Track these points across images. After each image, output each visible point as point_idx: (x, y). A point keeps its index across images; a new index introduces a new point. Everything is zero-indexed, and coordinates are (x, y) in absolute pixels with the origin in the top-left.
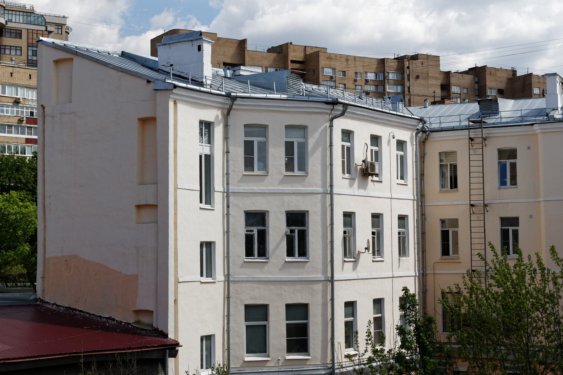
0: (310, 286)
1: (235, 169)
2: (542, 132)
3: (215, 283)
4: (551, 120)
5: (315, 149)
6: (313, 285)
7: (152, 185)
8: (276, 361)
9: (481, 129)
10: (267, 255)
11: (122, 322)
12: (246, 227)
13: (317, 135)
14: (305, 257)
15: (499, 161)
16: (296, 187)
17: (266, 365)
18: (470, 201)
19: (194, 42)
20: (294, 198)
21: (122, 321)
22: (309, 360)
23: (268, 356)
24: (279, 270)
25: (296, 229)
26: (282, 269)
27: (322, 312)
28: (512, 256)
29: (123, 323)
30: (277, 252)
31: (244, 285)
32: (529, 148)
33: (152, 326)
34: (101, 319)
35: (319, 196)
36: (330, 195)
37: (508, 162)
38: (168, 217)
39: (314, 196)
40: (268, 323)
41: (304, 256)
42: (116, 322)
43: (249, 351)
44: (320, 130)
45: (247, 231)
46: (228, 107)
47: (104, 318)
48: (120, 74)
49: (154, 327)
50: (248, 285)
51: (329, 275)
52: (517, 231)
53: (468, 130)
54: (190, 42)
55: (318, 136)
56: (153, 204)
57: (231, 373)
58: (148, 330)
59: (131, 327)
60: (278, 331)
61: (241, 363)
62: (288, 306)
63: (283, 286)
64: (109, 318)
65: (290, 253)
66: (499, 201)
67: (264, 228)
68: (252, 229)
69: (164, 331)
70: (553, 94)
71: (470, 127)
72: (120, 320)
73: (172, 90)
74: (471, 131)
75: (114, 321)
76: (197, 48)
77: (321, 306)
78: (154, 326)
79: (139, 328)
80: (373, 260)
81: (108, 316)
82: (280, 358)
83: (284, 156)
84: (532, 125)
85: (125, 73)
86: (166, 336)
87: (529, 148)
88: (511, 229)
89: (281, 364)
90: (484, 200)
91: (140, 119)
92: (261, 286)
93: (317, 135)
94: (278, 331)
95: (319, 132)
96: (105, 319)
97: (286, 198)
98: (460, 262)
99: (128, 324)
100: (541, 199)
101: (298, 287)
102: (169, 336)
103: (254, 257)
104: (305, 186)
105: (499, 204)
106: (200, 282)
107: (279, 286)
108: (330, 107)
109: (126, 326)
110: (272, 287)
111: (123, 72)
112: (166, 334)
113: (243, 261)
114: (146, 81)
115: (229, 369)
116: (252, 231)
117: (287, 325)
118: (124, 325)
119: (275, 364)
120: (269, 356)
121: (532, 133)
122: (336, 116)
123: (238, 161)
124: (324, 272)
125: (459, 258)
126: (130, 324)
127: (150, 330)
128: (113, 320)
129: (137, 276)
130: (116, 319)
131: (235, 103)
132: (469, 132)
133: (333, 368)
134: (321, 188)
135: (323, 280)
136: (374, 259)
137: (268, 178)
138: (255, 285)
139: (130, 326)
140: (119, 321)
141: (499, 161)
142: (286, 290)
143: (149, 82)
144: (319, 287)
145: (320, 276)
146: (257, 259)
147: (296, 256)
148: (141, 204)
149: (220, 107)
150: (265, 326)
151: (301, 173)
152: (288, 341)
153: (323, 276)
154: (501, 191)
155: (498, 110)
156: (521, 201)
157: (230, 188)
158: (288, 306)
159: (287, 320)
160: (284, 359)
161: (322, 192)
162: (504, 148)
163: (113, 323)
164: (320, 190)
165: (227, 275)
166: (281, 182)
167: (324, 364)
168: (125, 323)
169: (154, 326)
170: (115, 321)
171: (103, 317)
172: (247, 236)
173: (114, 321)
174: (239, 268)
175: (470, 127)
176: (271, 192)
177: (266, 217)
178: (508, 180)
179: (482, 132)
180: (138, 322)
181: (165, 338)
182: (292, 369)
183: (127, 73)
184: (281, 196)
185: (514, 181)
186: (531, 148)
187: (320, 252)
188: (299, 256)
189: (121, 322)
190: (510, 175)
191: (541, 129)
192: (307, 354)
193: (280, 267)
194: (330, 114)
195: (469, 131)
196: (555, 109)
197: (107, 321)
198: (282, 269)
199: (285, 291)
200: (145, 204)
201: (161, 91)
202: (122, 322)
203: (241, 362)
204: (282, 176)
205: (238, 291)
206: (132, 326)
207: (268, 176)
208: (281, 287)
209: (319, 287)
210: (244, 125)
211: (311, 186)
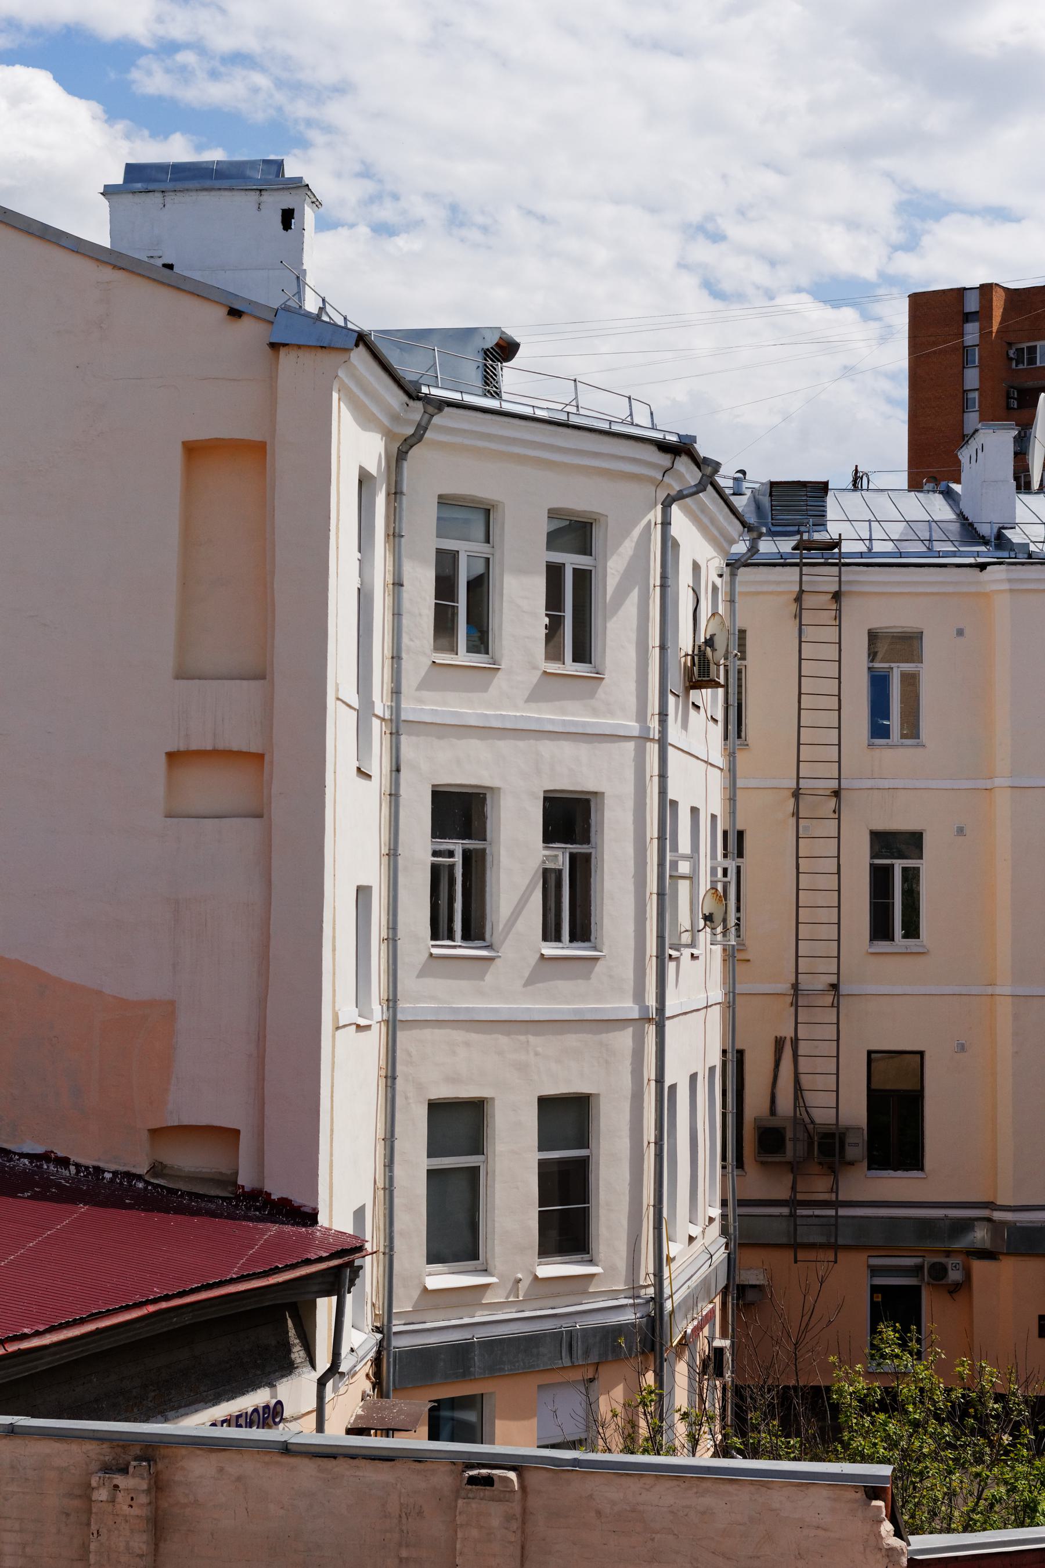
0: (604, 1037)
1: (412, 643)
2: (1011, 591)
3: (370, 1030)
4: (1020, 555)
5: (622, 593)
6: (611, 1035)
7: (245, 683)
8: (509, 1285)
9: (836, 569)
10: (488, 936)
11: (104, 1171)
12: (434, 840)
13: (628, 547)
14: (586, 944)
15: (871, 665)
16: (573, 715)
17: (483, 1302)
18: (798, 778)
19: (266, 197)
20: (567, 749)
21: (102, 1165)
22: (596, 1277)
23: (485, 1271)
24: (525, 985)
25: (457, 846)
26: (531, 980)
27: (630, 1121)
28: (900, 943)
29: (108, 1176)
30: (520, 925)
31: (427, 1033)
32: (960, 633)
33: (232, 1182)
34: (11, 1160)
35: (631, 745)
36: (656, 746)
37: (895, 670)
38: (324, 798)
39: (616, 745)
40: (486, 1161)
41: (583, 941)
42: (78, 1172)
43: (434, 1257)
44: (636, 532)
45: (435, 854)
46: (410, 431)
47: (23, 1155)
48: (108, 274)
49: (243, 1187)
50: (439, 1033)
51: (651, 1001)
52: (916, 871)
53: (797, 569)
54: (253, 193)
55: (630, 552)
56: (245, 749)
57: (395, 1333)
58: (218, 1197)
59: (146, 1188)
60: (517, 1188)
61: (416, 1297)
62: (544, 1102)
63: (532, 1039)
64: (46, 1157)
65: (551, 932)
66: (869, 784)
67: (481, 846)
68: (451, 847)
69: (298, 1199)
70: (1002, 481)
71: (804, 561)
72: (96, 1164)
73: (347, 350)
74: (805, 569)
75: (67, 1167)
76: (278, 218)
77: (629, 1101)
78: (240, 1182)
79: (178, 1190)
80: (692, 955)
81: (40, 1150)
82: (520, 1276)
83: (542, 611)
84: (982, 567)
85: (133, 272)
86: (311, 1218)
87: (960, 633)
88: (899, 865)
89: (523, 1297)
90: (839, 779)
91: (185, 444)
92: (474, 1037)
93: (628, 547)
94: (517, 1188)
95: (635, 540)
96: (26, 1161)
97: (547, 748)
98: (749, 961)
99: (129, 1176)
100: (998, 782)
101: (573, 1040)
102: (320, 1218)
103: (454, 941)
104: (595, 712)
105: (871, 791)
106: (354, 1027)
107: (522, 1038)
108: (665, 460)
109: (121, 1183)
110: (503, 1040)
111: (121, 268)
112: (308, 1210)
113: (427, 955)
114: (225, 311)
115: (390, 1321)
116: (451, 854)
117: (542, 1163)
118: (112, 1180)
119: (507, 1298)
120: (486, 1270)
121: (973, 589)
122: (685, 492)
123: (420, 615)
124: (639, 995)
125: (925, 951)
126: (139, 1177)
127: (224, 1199)
128: (64, 1162)
129: (172, 1003)
130: (73, 1158)
131: (436, 420)
132: (801, 575)
133: (658, 1300)
134: (636, 722)
135: (637, 1017)
136: (435, 951)
137: (500, 681)
138: (458, 1035)
139: (141, 1185)
140: (87, 1168)
141: (871, 665)
142: (539, 1049)
143: (235, 313)
144: (624, 1039)
145: (627, 1007)
146: (460, 946)
147: (563, 939)
148: (194, 747)
149: (384, 424)
150: (473, 1173)
151: (580, 669)
152: (544, 1218)
153: (636, 1007)
154: (877, 753)
155: (824, 516)
156: (933, 784)
157: (402, 706)
158: (544, 1102)
159: (541, 1149)
160: (531, 1278)
161: (637, 735)
162: (886, 628)
163: (66, 1173)
164: (633, 727)
165: (392, 1002)
166: (535, 696)
167: (634, 1290)
168: (115, 1173)
169: (240, 1182)
170: (73, 1168)
171: (15, 1153)
172: (435, 870)
173: (67, 1167)
174: (418, 977)
175: (804, 561)
176: (509, 725)
177: (488, 809)
178: (895, 722)
179: (840, 576)
180: (157, 1169)
181: (305, 1225)
182: (552, 1308)
183: (139, 275)
184: (532, 742)
185: (912, 729)
186: (966, 632)
187: (630, 928)
188: (571, 941)
189: (98, 1170)
190: (901, 707)
191: (1010, 581)
192: (586, 1257)
193: (527, 974)
194: (658, 484)
195: (801, 571)
196: (1006, 525)
197: (36, 1166)
198: (531, 980)
199: (537, 1054)
200: (209, 748)
201: (301, 353)
202: (104, 1171)
203: (416, 1294)
204: (535, 676)
205: (411, 1056)
206: (147, 1183)
207: (500, 671)
208: (528, 1042)
209: (624, 1039)
210: (440, 497)
211: (611, 713)
